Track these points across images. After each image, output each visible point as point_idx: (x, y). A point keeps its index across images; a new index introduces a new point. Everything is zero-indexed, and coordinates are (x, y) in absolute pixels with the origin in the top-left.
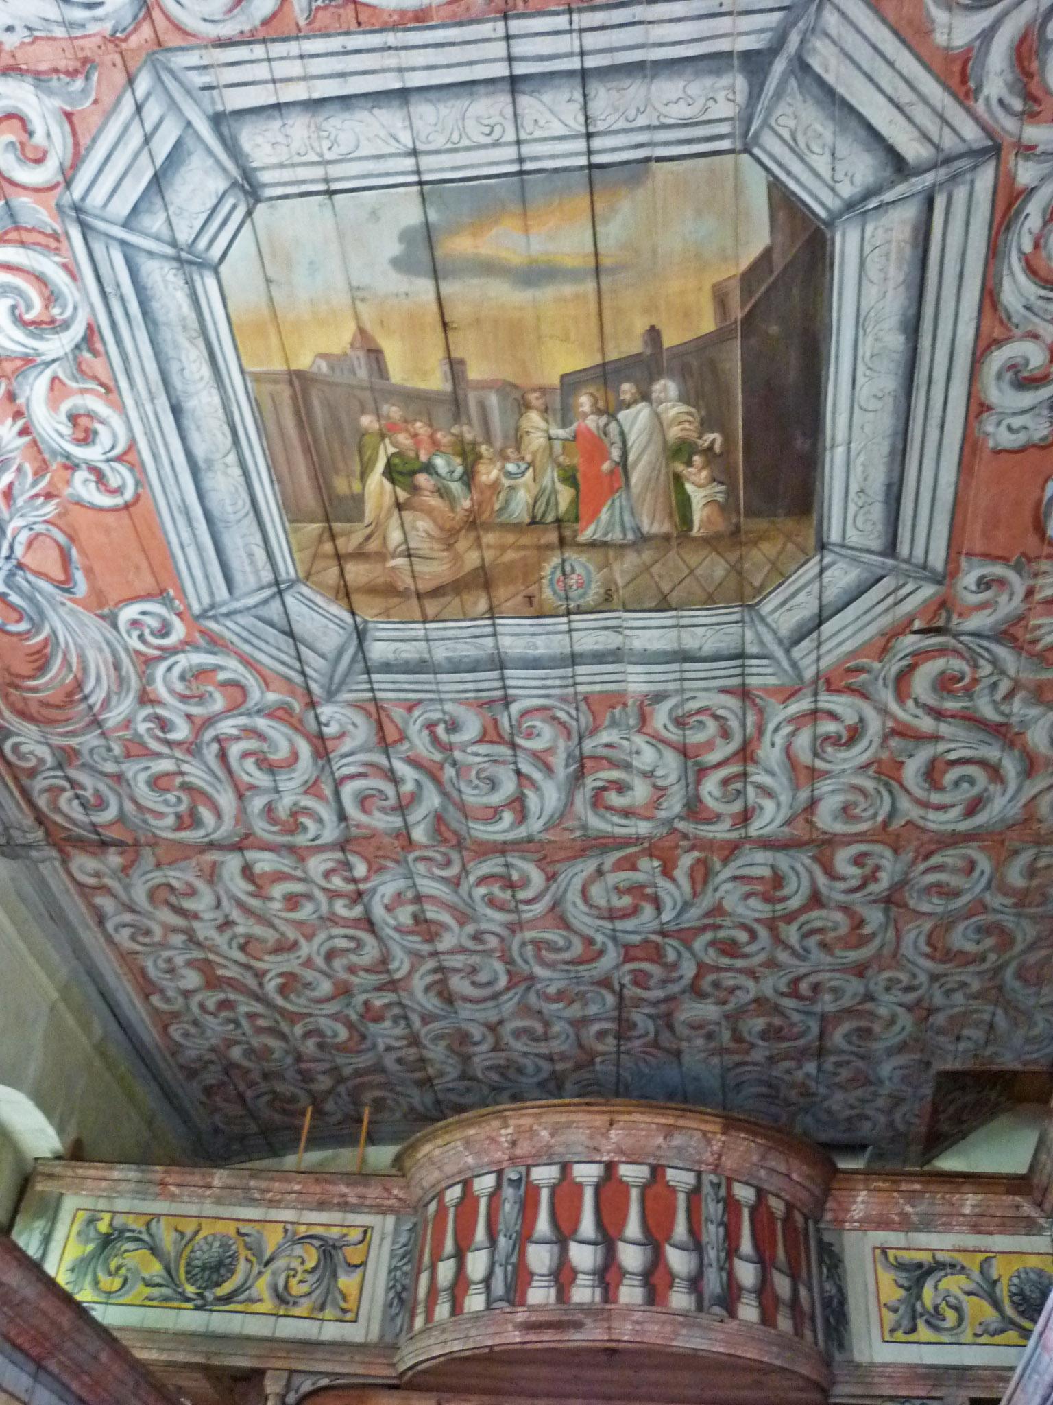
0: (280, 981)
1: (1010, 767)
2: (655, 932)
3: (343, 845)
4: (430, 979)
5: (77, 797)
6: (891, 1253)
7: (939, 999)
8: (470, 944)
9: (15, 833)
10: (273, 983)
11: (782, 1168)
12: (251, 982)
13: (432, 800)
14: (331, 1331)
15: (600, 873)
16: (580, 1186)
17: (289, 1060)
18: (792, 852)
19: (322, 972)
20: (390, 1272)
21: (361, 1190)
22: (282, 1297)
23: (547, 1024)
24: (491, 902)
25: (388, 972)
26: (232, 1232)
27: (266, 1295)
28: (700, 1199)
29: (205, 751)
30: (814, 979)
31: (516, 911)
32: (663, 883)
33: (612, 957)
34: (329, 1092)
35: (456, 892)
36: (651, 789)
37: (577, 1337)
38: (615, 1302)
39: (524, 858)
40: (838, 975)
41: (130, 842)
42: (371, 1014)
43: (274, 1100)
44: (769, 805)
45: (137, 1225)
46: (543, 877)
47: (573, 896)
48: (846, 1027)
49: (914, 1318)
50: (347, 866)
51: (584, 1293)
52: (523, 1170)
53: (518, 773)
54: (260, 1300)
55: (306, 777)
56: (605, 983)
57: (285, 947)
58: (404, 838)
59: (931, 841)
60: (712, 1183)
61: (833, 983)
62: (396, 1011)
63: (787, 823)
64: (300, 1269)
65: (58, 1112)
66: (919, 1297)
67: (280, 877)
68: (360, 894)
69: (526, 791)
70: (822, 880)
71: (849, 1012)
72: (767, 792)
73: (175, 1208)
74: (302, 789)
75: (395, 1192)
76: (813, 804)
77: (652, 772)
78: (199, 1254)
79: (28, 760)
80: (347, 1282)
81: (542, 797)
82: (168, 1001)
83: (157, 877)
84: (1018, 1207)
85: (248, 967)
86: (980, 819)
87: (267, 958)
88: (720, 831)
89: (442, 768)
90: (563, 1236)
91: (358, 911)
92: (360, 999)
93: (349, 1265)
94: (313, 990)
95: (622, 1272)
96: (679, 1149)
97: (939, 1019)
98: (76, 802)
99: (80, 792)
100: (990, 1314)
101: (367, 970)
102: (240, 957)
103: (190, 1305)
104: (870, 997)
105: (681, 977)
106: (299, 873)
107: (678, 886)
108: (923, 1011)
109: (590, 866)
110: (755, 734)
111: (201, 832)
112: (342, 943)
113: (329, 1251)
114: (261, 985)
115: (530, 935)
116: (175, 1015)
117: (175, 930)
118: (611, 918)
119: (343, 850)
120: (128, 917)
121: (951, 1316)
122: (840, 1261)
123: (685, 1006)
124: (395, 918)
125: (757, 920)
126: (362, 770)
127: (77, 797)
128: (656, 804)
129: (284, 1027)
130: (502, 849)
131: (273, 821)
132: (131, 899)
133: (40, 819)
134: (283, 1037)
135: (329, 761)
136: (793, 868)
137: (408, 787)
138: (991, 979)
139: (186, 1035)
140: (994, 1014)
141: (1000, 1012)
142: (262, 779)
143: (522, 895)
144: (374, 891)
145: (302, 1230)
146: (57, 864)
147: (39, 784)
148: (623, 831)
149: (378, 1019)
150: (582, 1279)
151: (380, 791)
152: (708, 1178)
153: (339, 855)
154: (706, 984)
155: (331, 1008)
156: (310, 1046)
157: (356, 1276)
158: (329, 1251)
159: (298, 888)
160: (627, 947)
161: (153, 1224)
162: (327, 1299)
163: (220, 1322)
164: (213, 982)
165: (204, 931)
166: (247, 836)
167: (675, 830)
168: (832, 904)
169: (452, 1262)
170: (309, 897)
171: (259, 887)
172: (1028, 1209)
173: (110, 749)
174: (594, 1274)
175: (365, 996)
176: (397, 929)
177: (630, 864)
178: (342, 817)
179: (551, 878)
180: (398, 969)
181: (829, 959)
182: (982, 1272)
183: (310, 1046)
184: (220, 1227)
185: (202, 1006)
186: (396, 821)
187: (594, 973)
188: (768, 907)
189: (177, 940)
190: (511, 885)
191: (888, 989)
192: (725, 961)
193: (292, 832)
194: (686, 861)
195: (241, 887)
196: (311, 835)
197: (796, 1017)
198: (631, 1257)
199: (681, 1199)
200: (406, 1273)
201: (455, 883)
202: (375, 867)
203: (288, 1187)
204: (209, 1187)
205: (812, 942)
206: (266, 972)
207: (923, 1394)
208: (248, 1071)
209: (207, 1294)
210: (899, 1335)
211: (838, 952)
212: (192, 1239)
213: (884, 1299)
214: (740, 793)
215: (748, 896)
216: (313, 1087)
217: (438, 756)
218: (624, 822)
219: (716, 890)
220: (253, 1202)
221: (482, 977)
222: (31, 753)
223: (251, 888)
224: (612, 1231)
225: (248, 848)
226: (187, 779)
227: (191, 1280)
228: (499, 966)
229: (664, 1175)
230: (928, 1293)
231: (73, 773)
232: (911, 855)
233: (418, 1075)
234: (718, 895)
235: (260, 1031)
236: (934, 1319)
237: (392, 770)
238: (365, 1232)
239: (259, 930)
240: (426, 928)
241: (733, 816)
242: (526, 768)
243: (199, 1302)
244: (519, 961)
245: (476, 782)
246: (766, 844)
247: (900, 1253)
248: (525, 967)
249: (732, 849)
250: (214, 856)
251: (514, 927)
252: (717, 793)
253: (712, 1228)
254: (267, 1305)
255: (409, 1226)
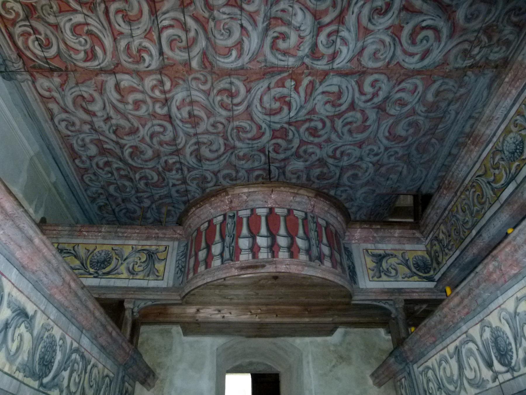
0: (130, 150)
1: (445, 32)
2: (286, 123)
3: (161, 71)
4: (193, 148)
5: (37, 39)
6: (369, 251)
7: (385, 160)
8: (211, 129)
9: (9, 64)
10: (127, 152)
11: (335, 215)
12: (118, 151)
13: (202, 43)
14: (153, 284)
15: (269, 88)
16: (260, 217)
17: (133, 192)
18: (348, 78)
19: (149, 145)
20: (177, 261)
21: (164, 231)
22: (132, 272)
23: (237, 172)
24: (222, 105)
25: (176, 145)
26: (110, 249)
27: (124, 271)
28: (307, 222)
29: (98, 9)
30: (342, 149)
31: (232, 110)
32: (294, 95)
33: (268, 135)
34: (149, 208)
35: (208, 99)
36: (298, 38)
37: (263, 271)
38: (278, 257)
39: (238, 79)
40: (352, 147)
41: (64, 69)
42: (168, 168)
43: (127, 212)
44: (344, 49)
45: (70, 248)
46: (245, 90)
47: (256, 102)
48: (350, 173)
49: (380, 272)
50: (162, 83)
51: (263, 255)
52: (235, 212)
53: (242, 26)
54: (122, 273)
55: (145, 27)
56: (262, 150)
57: (134, 131)
58: (187, 64)
59: (404, 74)
60: (311, 217)
61: (349, 151)
62: (178, 166)
63: (350, 61)
64: (139, 262)
65: (35, 203)
66: (381, 265)
67: (133, 90)
68: (166, 100)
69: (244, 39)
70: (357, 95)
71: (352, 166)
72: (345, 42)
73: (85, 241)
74: (143, 36)
75: (178, 232)
76: (363, 49)
77: (299, 27)
78: (96, 257)
79: (11, 13)
80: (159, 266)
81: (250, 42)
82: (83, 162)
83: (76, 91)
84: (414, 234)
85: (117, 143)
86: (426, 62)
87: (125, 137)
88: (321, 65)
89: (208, 22)
90: (253, 235)
91: (165, 111)
92: (164, 159)
93: (159, 259)
94: (144, 155)
95: (279, 247)
96: (299, 203)
97: (383, 170)
98: (36, 43)
99: (38, 36)
100: (407, 270)
101: (167, 144)
102: (113, 137)
103: (92, 276)
104: (361, 159)
105: (293, 147)
106: (140, 88)
107: (300, 97)
108: (378, 165)
109: (264, 84)
110: (346, 6)
111: (96, 63)
112: (158, 129)
113: (151, 256)
114: (122, 153)
115: (236, 123)
116: (86, 170)
117: (85, 122)
118: (270, 115)
119: (161, 73)
120: (64, 116)
121: (393, 272)
122: (351, 253)
123: (292, 162)
124: (181, 114)
125: (327, 117)
126: (172, 23)
127: (37, 39)
128: (298, 47)
129: (131, 175)
130: (229, 73)
131: (130, 55)
132: (65, 104)
133: (20, 55)
134: (131, 180)
135: (157, 17)
136: (347, 87)
137: (192, 34)
138: (407, 150)
139: (91, 180)
140: (403, 168)
141: (405, 166)
142: (125, 28)
143: (236, 101)
144: (173, 97)
145: (140, 248)
146: (30, 83)
147: (18, 30)
148: (282, 63)
149: (170, 170)
150: (262, 250)
151: (179, 37)
152: (309, 215)
153: (158, 77)
154: (301, 151)
155: (151, 164)
156: (142, 185)
157: (163, 263)
158: (151, 256)
159: (139, 96)
160: (274, 131)
161: (76, 247)
162: (151, 272)
163: (103, 282)
164: (103, 152)
165: (99, 123)
166: (117, 65)
167: (303, 63)
168: (358, 109)
169: (205, 251)
170: (144, 102)
171: (123, 96)
172: (418, 235)
173: (51, 8)
174: (268, 248)
175: (166, 158)
176: (181, 121)
177: (281, 84)
178: (161, 53)
179: (248, 91)
180: (180, 144)
181: (350, 139)
182: (402, 257)
183: (142, 185)
184: (105, 248)
185: (97, 165)
186: (185, 56)
187: (259, 145)
188: (333, 109)
189: (86, 128)
190: (232, 96)
191: (368, 154)
192: (311, 139)
193: (138, 62)
194: (305, 82)
195: (114, 96)
196: (146, 64)
197: (332, 168)
198: (282, 241)
199: (300, 221)
200: (183, 262)
201: (207, 93)
202: (174, 83)
203: (134, 231)
204: (100, 232)
205: (346, 128)
206: (125, 145)
207: (386, 298)
208: (116, 198)
209: (99, 272)
210: (375, 279)
211: (355, 135)
212: (93, 252)
213: (368, 267)
214: (334, 42)
215: (326, 103)
216: (142, 205)
217: (207, 15)
218: (283, 58)
219: (314, 100)
220: (119, 237)
221: (214, 147)
222: (12, 8)
223: (119, 97)
224: (274, 232)
225: (118, 73)
226: (90, 28)
227: (92, 266)
228: (221, 141)
229: (293, 212)
230: (384, 265)
231: (35, 24)
232: (394, 81)
233: (185, 199)
234: (315, 102)
235: (121, 177)
236: (387, 273)
237: (185, 23)
238: (166, 248)
239: (123, 122)
240: (193, 120)
241: (329, 56)
242: (246, 24)
243: (96, 275)
244: (230, 138)
245: (223, 31)
246: (340, 73)
247: (372, 251)
248: (232, 142)
249: (325, 74)
250: (102, 77)
251: (229, 119)
252: (325, 42)
253: (313, 232)
254: (125, 275)
255: (184, 244)
